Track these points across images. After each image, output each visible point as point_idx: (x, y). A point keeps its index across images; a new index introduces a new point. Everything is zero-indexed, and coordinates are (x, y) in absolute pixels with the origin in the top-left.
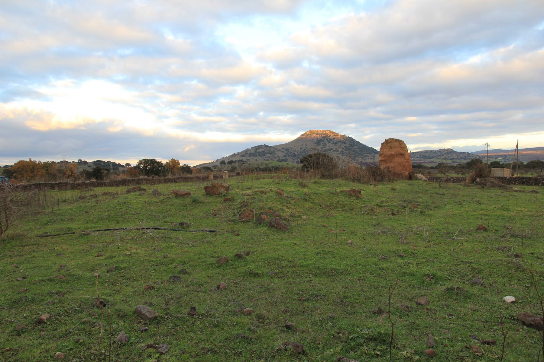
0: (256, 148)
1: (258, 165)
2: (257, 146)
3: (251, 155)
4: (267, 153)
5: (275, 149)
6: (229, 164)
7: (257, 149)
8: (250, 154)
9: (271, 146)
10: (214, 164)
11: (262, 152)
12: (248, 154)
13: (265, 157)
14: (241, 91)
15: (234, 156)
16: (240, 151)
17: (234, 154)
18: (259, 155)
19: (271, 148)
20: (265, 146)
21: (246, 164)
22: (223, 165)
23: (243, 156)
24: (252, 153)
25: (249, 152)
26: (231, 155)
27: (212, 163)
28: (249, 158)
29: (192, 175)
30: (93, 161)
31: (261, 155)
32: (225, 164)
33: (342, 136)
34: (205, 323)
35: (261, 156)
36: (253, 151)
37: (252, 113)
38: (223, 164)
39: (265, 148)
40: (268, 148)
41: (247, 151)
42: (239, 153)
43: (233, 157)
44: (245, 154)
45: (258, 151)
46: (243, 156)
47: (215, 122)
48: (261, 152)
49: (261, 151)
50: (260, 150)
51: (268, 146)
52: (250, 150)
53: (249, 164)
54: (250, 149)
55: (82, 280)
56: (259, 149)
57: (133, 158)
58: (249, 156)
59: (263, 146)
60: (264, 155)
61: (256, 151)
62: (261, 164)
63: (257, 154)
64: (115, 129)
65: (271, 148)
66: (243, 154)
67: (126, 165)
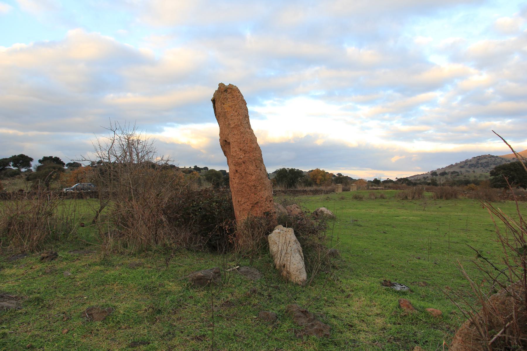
0: (478, 158)
1: (475, 177)
2: (480, 156)
3: (471, 166)
4: (491, 164)
5: (503, 159)
6: (442, 176)
7: (479, 159)
8: (470, 165)
9: (497, 157)
10: (424, 176)
11: (485, 162)
12: (468, 165)
13: (489, 169)
14: (438, 96)
15: (451, 168)
16: (459, 162)
17: (452, 165)
18: (481, 166)
19: (496, 158)
20: (490, 156)
21: (460, 176)
22: (434, 176)
23: (462, 167)
24: (473, 164)
25: (469, 163)
26: (448, 165)
27: (426, 174)
28: (468, 170)
29: (312, 188)
30: (309, 170)
31: (484, 166)
32: (437, 175)
33: (18, 156)
34: (21, 313)
35: (483, 167)
36: (474, 162)
37: (462, 119)
38: (435, 175)
39: (490, 159)
40: (493, 159)
41: (466, 162)
42: (457, 164)
43: (450, 168)
44: (464, 165)
45: (480, 162)
46: (462, 167)
47: (420, 132)
48: (484, 163)
49: (484, 162)
50: (484, 161)
51: (493, 156)
52: (471, 161)
53: (465, 176)
54: (471, 160)
55: (333, 273)
56: (481, 159)
57: (344, 168)
58: (469, 168)
59: (486, 156)
60: (487, 166)
61: (477, 162)
62: (480, 177)
63: (480, 165)
64: (319, 142)
65: (496, 158)
66: (462, 165)
67: (337, 174)
